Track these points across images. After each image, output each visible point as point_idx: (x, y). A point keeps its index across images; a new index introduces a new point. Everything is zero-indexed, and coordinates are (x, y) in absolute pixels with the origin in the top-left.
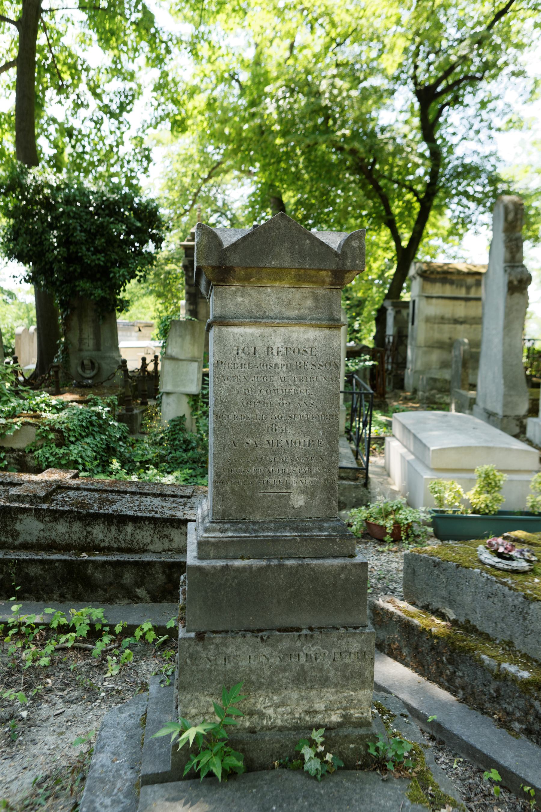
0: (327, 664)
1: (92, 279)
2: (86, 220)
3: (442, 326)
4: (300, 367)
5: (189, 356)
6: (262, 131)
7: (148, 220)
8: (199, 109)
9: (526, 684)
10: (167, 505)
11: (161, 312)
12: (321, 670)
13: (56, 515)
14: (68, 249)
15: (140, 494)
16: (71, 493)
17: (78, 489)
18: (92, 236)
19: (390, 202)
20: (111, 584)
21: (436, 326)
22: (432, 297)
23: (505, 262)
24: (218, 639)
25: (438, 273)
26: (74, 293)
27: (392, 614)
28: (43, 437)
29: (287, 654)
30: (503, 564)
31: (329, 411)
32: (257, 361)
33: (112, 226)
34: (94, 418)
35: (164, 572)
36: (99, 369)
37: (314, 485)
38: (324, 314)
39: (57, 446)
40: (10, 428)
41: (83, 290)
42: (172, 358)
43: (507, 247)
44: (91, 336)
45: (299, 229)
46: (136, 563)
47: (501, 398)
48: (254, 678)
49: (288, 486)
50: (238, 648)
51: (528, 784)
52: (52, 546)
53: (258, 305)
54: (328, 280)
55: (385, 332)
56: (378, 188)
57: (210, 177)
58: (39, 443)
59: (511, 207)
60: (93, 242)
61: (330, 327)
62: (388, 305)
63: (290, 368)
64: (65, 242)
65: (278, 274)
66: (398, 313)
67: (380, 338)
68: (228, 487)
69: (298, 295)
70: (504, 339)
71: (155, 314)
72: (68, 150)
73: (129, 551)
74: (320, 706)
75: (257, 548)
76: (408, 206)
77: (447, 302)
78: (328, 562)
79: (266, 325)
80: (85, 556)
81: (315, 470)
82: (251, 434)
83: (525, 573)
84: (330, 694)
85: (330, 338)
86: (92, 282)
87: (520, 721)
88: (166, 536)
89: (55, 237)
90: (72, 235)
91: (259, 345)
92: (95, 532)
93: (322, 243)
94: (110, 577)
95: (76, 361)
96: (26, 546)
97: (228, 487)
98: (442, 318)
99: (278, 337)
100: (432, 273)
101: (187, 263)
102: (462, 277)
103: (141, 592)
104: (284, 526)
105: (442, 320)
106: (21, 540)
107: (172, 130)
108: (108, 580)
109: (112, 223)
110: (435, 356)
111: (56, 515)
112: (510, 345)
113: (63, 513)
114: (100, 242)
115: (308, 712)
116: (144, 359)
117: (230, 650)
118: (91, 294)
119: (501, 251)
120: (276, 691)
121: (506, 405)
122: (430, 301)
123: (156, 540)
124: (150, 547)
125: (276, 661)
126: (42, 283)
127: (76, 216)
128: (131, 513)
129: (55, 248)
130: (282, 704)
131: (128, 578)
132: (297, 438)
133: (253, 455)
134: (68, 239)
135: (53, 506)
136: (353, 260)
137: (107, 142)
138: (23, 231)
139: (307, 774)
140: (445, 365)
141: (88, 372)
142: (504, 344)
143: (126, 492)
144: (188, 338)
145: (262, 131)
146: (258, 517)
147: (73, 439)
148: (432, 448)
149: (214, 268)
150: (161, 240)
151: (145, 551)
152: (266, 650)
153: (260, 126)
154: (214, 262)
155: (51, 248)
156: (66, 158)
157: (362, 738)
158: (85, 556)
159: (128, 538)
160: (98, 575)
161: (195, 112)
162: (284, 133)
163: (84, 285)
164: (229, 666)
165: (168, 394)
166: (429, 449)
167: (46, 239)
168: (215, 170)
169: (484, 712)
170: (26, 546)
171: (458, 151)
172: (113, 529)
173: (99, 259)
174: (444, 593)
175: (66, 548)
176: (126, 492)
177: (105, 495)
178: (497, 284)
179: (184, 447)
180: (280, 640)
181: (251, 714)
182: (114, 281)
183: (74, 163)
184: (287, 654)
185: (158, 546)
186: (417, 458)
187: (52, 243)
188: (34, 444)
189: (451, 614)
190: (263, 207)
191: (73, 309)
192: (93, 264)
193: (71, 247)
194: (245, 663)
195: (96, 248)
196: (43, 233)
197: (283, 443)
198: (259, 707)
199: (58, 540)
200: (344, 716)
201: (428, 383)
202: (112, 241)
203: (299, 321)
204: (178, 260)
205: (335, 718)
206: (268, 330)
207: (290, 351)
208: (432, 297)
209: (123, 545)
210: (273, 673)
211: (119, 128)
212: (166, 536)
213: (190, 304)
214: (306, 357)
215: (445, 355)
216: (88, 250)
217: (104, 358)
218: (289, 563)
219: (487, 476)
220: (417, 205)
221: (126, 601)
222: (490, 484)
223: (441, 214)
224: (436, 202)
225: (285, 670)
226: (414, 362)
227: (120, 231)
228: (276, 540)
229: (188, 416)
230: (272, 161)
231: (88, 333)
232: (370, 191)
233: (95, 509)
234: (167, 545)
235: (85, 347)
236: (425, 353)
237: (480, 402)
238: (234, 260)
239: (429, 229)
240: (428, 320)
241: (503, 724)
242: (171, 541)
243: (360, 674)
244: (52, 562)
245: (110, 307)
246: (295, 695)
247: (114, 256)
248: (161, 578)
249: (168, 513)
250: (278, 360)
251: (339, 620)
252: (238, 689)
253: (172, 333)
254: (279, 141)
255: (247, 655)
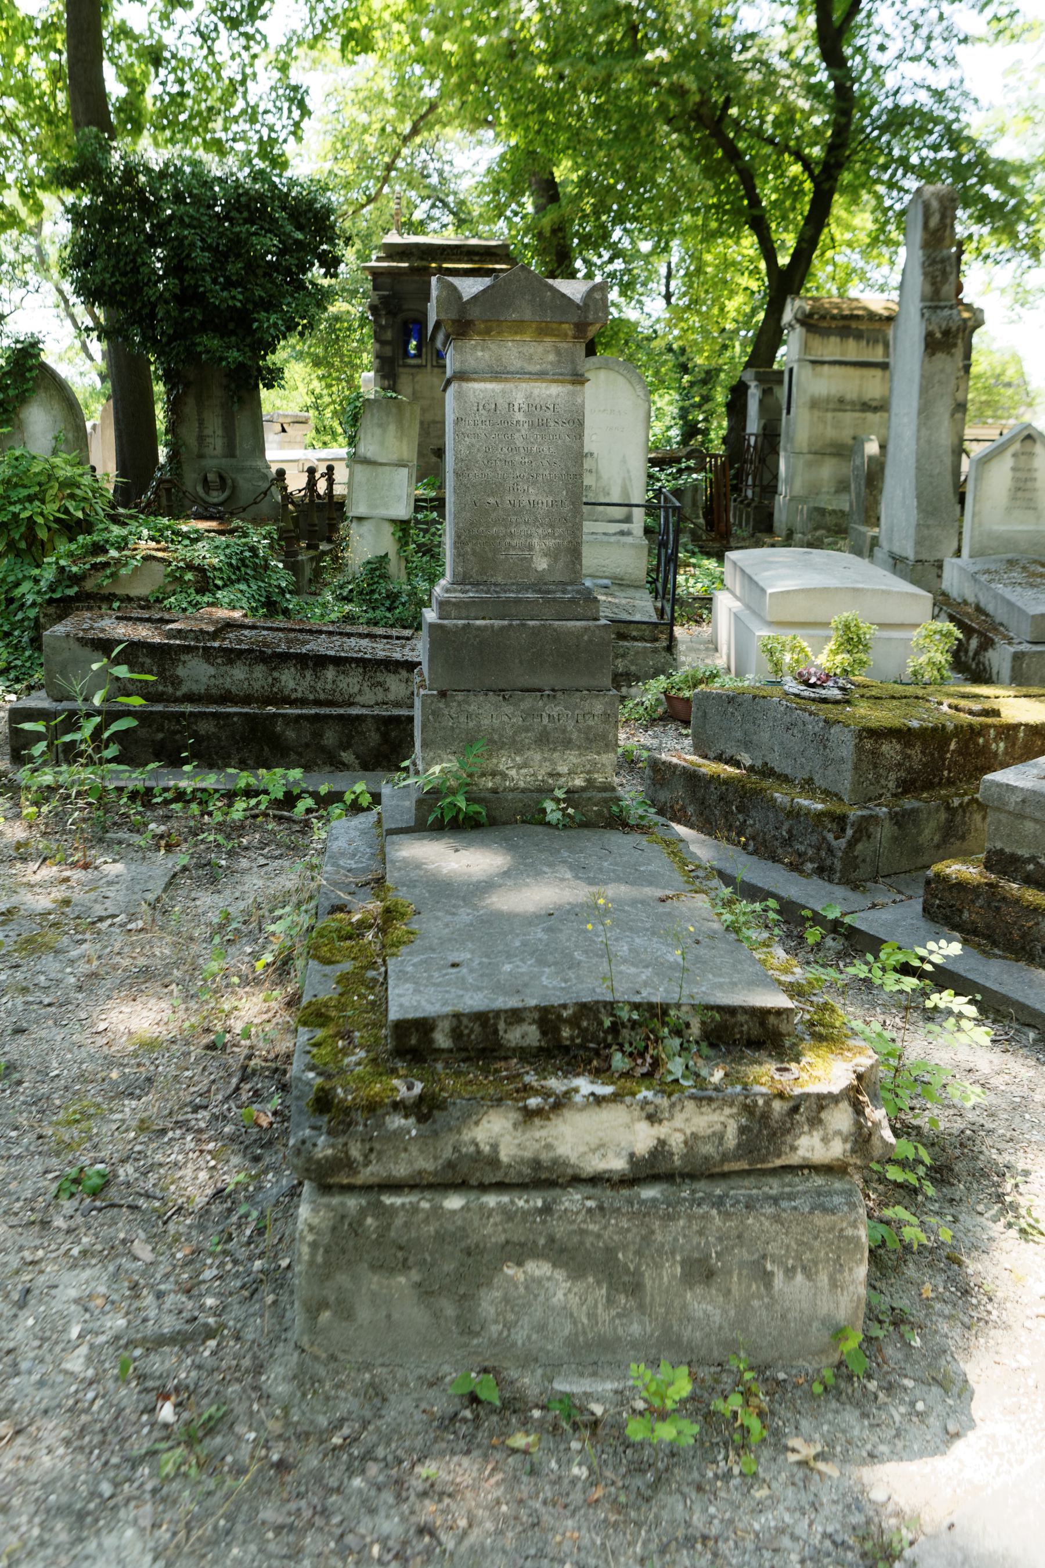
0: (570, 725)
1: (222, 332)
2: (210, 229)
3: (840, 414)
4: (542, 424)
5: (394, 457)
6: (513, 52)
7: (308, 224)
8: (393, 9)
9: (820, 814)
10: (380, 646)
11: (319, 397)
12: (564, 731)
13: (231, 656)
14: (182, 281)
15: (340, 634)
16: (246, 632)
17: (253, 627)
18: (221, 256)
19: (758, 182)
20: (307, 745)
21: (829, 415)
22: (823, 363)
23: (923, 299)
24: (460, 697)
25: (834, 317)
26: (192, 356)
27: (676, 766)
28: (176, 579)
29: (529, 714)
30: (808, 693)
31: (573, 470)
32: (498, 418)
33: (254, 240)
34: (247, 554)
35: (378, 729)
36: (234, 488)
37: (558, 548)
38: (566, 369)
39: (197, 592)
40: (126, 565)
41: (208, 352)
42: (367, 462)
43: (925, 274)
44: (220, 432)
45: (320, 507)
46: (341, 717)
47: (912, 531)
48: (496, 737)
49: (531, 548)
50: (480, 707)
51: (804, 907)
52: (226, 698)
53: (499, 359)
54: (570, 333)
55: (744, 428)
56: (733, 154)
57: (415, 131)
58: (170, 588)
59: (935, 204)
60: (223, 269)
61: (573, 383)
62: (749, 377)
63: (532, 425)
64: (176, 267)
65: (519, 326)
66: (767, 392)
67: (735, 438)
68: (468, 549)
69: (540, 349)
70: (919, 430)
71: (309, 400)
72: (153, 89)
73: (330, 703)
74: (563, 769)
75: (499, 608)
76: (792, 191)
77: (850, 371)
78: (571, 624)
79: (506, 380)
80: (272, 709)
81: (559, 531)
82: (492, 494)
83: (837, 702)
84: (573, 757)
85: (573, 394)
86: (222, 337)
87: (812, 861)
88: (380, 684)
89: (159, 260)
90: (189, 255)
91: (500, 401)
92: (283, 678)
93: (564, 295)
94: (306, 737)
95: (195, 476)
96: (190, 698)
97: (468, 549)
98: (841, 401)
99: (520, 393)
100: (823, 317)
101: (377, 302)
102: (877, 325)
103: (347, 756)
104: (527, 588)
105: (841, 404)
106: (184, 689)
107: (343, 50)
108: (304, 740)
109: (255, 234)
110: (828, 471)
111: (231, 656)
112: (929, 442)
113: (241, 652)
114: (234, 268)
115: (551, 775)
116: (311, 471)
117: (472, 708)
118: (221, 359)
119: (917, 283)
120: (518, 752)
121: (919, 543)
122: (819, 368)
123: (366, 689)
124: (358, 699)
125: (518, 720)
126: (137, 339)
127: (195, 224)
128: (332, 653)
129: (160, 279)
130: (525, 765)
131: (330, 737)
132: (540, 498)
133: (494, 515)
134: (181, 261)
135: (226, 644)
136: (596, 313)
137: (225, 74)
138: (103, 248)
139: (549, 824)
140: (842, 487)
141: (215, 493)
142: (918, 439)
143: (321, 632)
144: (392, 428)
145: (513, 52)
146: (500, 580)
147: (219, 583)
148: (769, 591)
149: (454, 321)
150: (337, 261)
151: (351, 704)
152: (508, 709)
153: (510, 42)
154: (454, 316)
155: (154, 278)
156: (149, 103)
157: (606, 801)
158: (272, 709)
159: (329, 687)
160: (291, 734)
161: (387, 16)
162: (552, 58)
163: (210, 342)
164: (471, 724)
165: (360, 519)
166: (763, 591)
167: (144, 264)
168: (425, 119)
169: (775, 859)
170: (190, 698)
171: (891, 80)
172: (308, 674)
173: (233, 298)
174: (739, 734)
175: (247, 700)
176: (321, 632)
177: (292, 635)
178: (909, 339)
179: (388, 603)
180: (522, 700)
181: (494, 774)
182: (258, 335)
183: (163, 113)
184: (529, 714)
185: (369, 697)
186: (748, 607)
187: (154, 271)
188: (162, 589)
189: (747, 760)
190: (515, 194)
191: (187, 385)
192: (224, 306)
193: (187, 277)
194: (486, 722)
195: (227, 278)
196: (137, 253)
197: (525, 503)
198: (502, 767)
199: (234, 689)
200: (588, 780)
201: (810, 519)
202: (254, 265)
203: (541, 376)
204: (354, 293)
205: (579, 782)
206: (509, 386)
207: (532, 408)
208: (823, 363)
209: (322, 696)
210: (515, 733)
211: (247, 48)
212: (380, 684)
213: (383, 377)
214: (549, 414)
215: (845, 469)
216: (215, 281)
217: (241, 470)
218: (531, 623)
219: (847, 627)
220: (808, 185)
221: (327, 769)
222: (852, 641)
223: (855, 200)
224: (846, 177)
225: (527, 730)
226: (790, 481)
227: (268, 248)
228: (517, 601)
229: (392, 556)
230: (530, 108)
231: (214, 426)
232: (719, 161)
233: (283, 648)
234: (380, 697)
235: (209, 451)
236: (809, 465)
237: (884, 542)
238: (474, 313)
239: (834, 229)
240: (815, 404)
241: (795, 867)
242: (387, 690)
243: (604, 737)
244: (229, 714)
245: (250, 378)
246: (538, 757)
247: (259, 292)
248: (374, 738)
249: (381, 654)
250: (519, 416)
251: (584, 682)
252: (479, 748)
253: (367, 422)
254: (541, 70)
255: (489, 714)
